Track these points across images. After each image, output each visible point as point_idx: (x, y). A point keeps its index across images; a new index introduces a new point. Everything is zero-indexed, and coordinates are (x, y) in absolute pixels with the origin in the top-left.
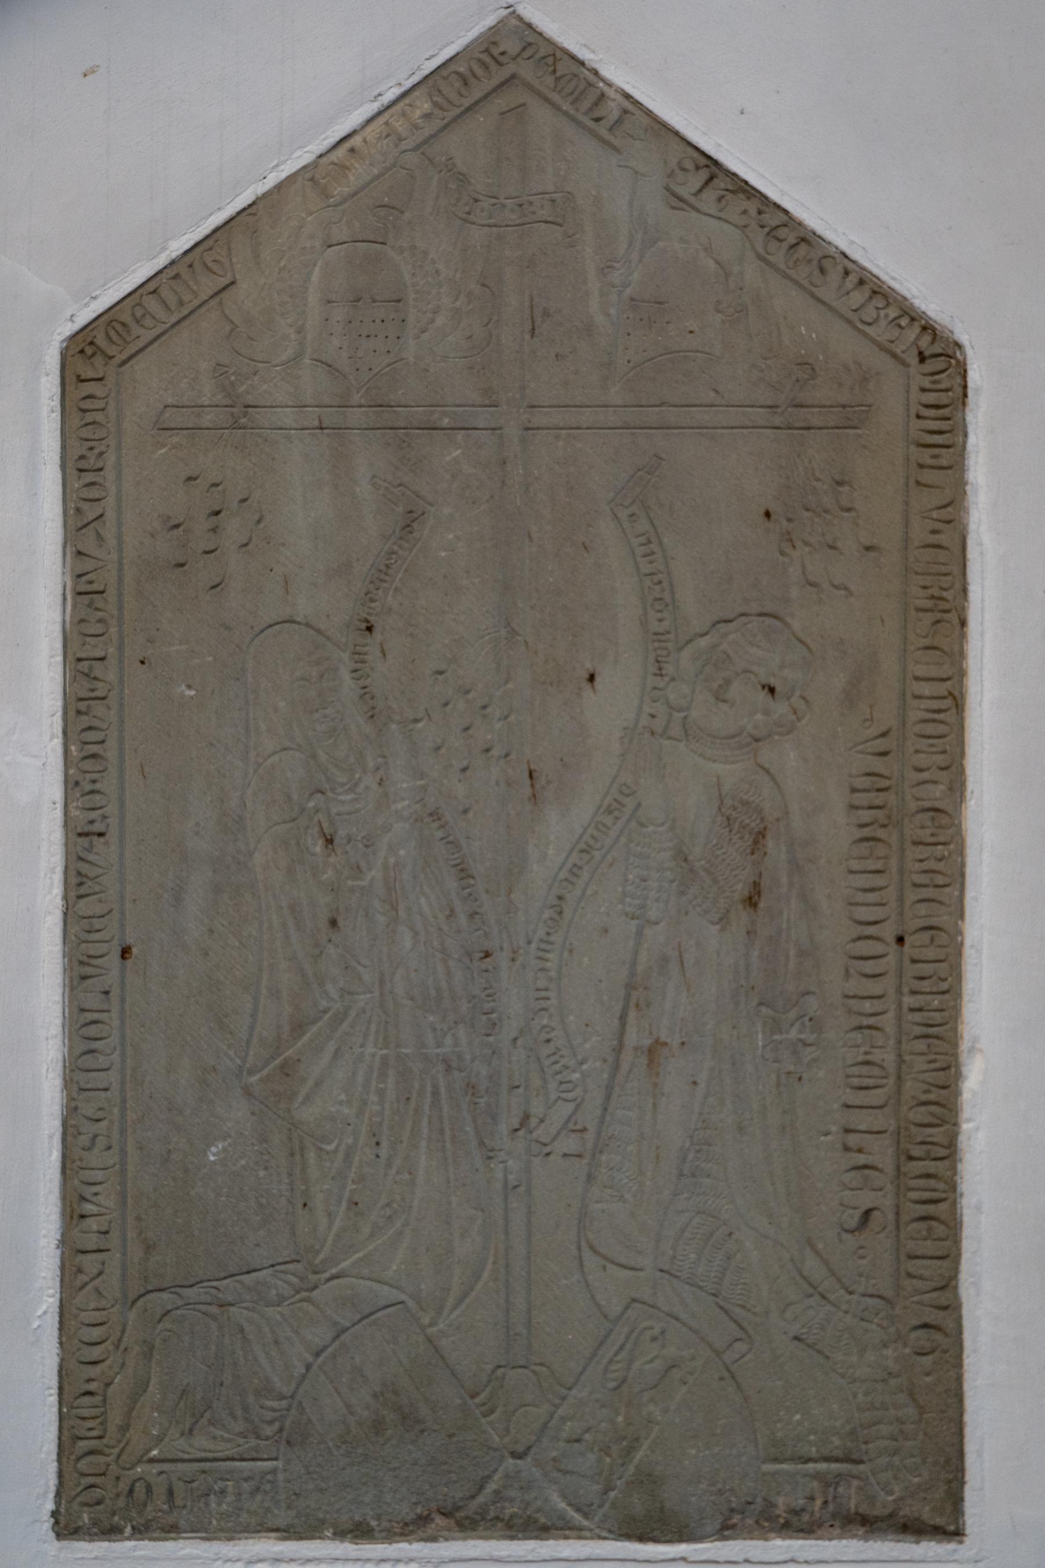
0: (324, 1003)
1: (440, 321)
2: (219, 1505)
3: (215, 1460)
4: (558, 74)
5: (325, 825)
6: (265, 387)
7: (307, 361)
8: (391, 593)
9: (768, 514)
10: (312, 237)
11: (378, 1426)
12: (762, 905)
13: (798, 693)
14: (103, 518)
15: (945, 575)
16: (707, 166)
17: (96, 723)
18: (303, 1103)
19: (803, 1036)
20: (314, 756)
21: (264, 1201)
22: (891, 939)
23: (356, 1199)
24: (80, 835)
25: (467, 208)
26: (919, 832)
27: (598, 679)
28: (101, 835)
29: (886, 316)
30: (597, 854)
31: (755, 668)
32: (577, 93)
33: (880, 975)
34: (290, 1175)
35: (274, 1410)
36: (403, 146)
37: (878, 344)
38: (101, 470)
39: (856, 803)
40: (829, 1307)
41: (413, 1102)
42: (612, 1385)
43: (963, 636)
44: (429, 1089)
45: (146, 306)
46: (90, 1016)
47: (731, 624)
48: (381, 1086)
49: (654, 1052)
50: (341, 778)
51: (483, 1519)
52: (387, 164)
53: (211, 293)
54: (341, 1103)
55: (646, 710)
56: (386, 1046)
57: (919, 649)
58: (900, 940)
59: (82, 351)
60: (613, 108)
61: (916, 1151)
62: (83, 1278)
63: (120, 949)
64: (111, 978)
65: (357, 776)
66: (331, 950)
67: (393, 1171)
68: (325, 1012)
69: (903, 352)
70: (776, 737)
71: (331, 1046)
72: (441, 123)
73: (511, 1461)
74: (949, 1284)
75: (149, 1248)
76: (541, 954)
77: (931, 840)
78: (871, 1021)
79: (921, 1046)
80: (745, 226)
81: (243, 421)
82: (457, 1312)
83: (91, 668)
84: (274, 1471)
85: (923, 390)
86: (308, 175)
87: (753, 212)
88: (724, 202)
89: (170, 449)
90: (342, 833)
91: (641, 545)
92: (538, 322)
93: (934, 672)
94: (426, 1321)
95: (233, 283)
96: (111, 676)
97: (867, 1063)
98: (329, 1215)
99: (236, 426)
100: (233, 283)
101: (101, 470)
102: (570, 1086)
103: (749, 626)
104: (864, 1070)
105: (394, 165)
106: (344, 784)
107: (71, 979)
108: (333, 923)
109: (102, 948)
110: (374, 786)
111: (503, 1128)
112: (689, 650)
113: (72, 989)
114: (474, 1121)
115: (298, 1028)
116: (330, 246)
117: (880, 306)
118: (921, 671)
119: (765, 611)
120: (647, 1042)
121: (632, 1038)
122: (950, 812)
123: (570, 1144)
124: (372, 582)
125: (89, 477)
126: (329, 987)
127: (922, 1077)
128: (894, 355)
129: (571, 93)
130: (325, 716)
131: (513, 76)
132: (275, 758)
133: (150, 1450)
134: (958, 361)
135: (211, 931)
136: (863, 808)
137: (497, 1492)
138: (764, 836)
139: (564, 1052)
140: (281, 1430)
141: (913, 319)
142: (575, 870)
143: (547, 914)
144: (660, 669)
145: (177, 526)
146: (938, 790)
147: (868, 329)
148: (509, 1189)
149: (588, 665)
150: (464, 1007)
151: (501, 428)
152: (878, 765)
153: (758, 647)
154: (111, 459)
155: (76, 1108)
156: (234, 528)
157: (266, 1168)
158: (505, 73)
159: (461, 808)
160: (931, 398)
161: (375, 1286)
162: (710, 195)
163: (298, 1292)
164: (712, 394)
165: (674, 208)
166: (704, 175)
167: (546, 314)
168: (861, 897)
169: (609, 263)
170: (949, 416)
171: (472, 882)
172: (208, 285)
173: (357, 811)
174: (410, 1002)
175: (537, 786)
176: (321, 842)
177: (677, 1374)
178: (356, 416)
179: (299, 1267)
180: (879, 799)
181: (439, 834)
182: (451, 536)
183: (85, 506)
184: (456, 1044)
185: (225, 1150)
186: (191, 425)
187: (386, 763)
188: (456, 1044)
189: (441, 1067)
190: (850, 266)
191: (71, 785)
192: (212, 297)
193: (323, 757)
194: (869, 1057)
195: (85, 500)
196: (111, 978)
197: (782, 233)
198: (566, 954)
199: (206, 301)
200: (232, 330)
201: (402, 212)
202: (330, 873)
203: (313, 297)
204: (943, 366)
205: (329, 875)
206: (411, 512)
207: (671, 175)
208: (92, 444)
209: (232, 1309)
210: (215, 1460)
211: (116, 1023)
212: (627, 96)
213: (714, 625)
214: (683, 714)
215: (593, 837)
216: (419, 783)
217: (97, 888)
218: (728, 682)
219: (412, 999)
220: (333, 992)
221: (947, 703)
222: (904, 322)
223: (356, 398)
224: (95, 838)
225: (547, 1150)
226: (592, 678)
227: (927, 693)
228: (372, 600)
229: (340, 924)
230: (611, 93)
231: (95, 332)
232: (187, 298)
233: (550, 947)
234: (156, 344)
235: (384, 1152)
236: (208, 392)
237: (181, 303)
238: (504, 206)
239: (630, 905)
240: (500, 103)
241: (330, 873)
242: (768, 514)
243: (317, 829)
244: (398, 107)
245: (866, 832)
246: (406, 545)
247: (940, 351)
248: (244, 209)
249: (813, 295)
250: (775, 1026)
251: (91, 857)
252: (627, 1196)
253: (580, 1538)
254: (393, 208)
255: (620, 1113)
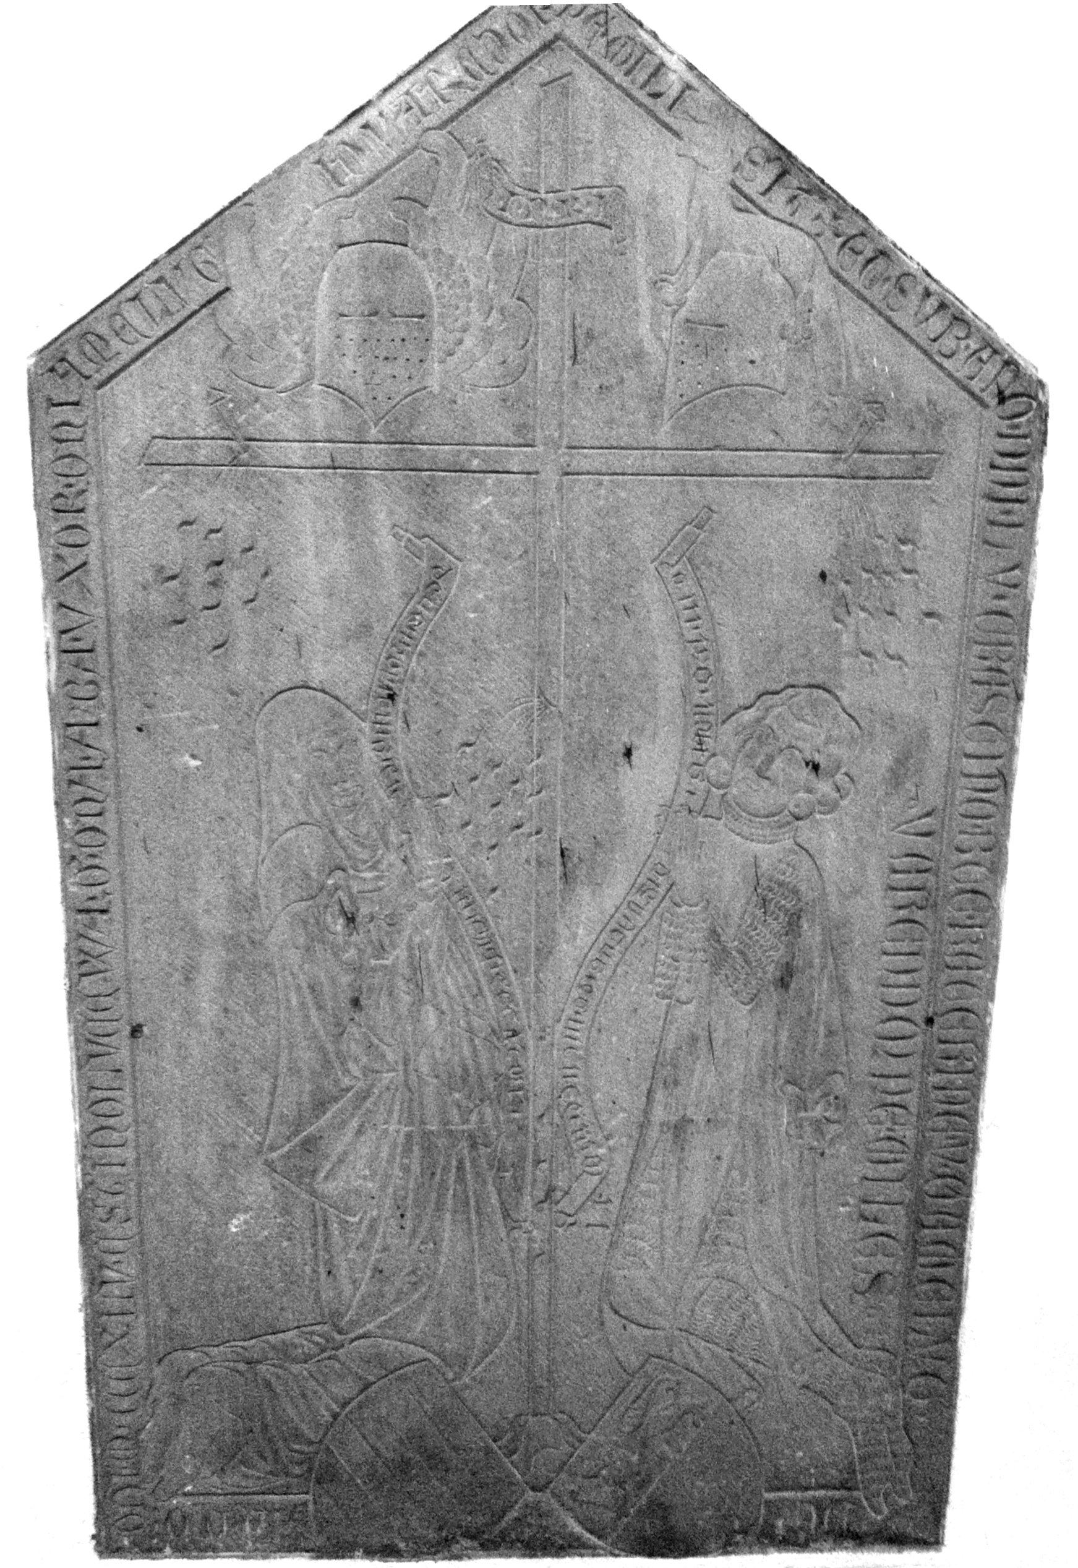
0: (346, 1082)
1: (469, 342)
2: (253, 1529)
3: (248, 1494)
4: (612, 35)
5: (347, 904)
6: (268, 417)
7: (316, 387)
8: (414, 659)
9: (823, 576)
10: (319, 235)
11: (404, 1466)
12: (793, 986)
13: (843, 770)
14: (87, 567)
15: (1004, 645)
16: (779, 159)
17: (91, 793)
18: (326, 1178)
19: (827, 1114)
20: (333, 832)
21: (287, 1269)
22: (920, 1020)
23: (381, 1266)
24: (80, 911)
25: (501, 203)
26: (956, 914)
27: (635, 754)
28: (103, 911)
29: (967, 347)
30: (629, 935)
31: (800, 744)
32: (632, 61)
33: (906, 1055)
34: (313, 1245)
35: (302, 1453)
36: (427, 122)
37: (957, 382)
38: (82, 510)
39: (894, 884)
40: (835, 1359)
41: (438, 1177)
42: (627, 1429)
43: (1017, 711)
44: (454, 1163)
45: (126, 315)
46: (100, 1094)
47: (777, 697)
48: (406, 1161)
49: (679, 1129)
50: (364, 855)
51: (504, 1540)
52: (408, 146)
53: (202, 302)
54: (365, 1178)
55: (684, 786)
56: (412, 1124)
57: (972, 725)
58: (930, 1021)
59: (52, 370)
60: (672, 82)
61: (931, 1220)
62: (107, 1338)
63: (128, 1028)
64: (123, 1056)
65: (380, 852)
66: (354, 1029)
67: (418, 1242)
68: (348, 1090)
69: (983, 390)
70: (818, 816)
71: (354, 1123)
72: (471, 95)
73: (531, 1493)
74: (950, 1337)
75: (173, 1311)
76: (568, 1032)
77: (969, 922)
78: (896, 1099)
79: (941, 1122)
80: (818, 235)
81: (245, 456)
82: (479, 1368)
83: (82, 734)
84: (305, 1504)
85: (1001, 435)
86: (313, 157)
87: (827, 216)
88: (796, 203)
89: (160, 489)
90: (364, 910)
91: (686, 608)
92: (580, 346)
93: (982, 750)
94: (450, 1375)
95: (227, 289)
96: (107, 744)
97: (889, 1138)
98: (354, 1282)
99: (235, 462)
100: (227, 289)
101: (82, 510)
102: (596, 1160)
103: (795, 699)
104: (886, 1145)
105: (416, 147)
106: (366, 862)
107: (78, 1058)
108: (356, 1003)
109: (110, 1027)
110: (399, 863)
111: (527, 1201)
112: (729, 727)
113: (80, 1067)
114: (499, 1194)
115: (320, 1105)
116: (341, 247)
117: (962, 335)
118: (970, 747)
119: (813, 682)
120: (673, 1119)
121: (659, 1114)
122: (988, 892)
123: (594, 1215)
124: (393, 645)
125: (69, 519)
126: (351, 1065)
127: (940, 1151)
128: (972, 394)
129: (625, 62)
130: (344, 790)
131: (557, 37)
132: (290, 835)
133: (185, 1485)
134: (1040, 404)
135: (226, 1010)
136: (902, 889)
137: (517, 1519)
138: (799, 918)
139: (591, 1128)
140: (310, 1470)
141: (995, 352)
142: (606, 950)
143: (575, 993)
144: (701, 744)
145: (173, 577)
146: (978, 872)
147: (946, 363)
148: (532, 1258)
149: (625, 739)
150: (491, 1085)
151: (537, 473)
152: (921, 844)
153: (806, 721)
154: (92, 498)
155: (92, 1183)
156: (237, 584)
157: (289, 1239)
158: (547, 34)
159: (489, 886)
160: (1008, 445)
161: (403, 1346)
162: (780, 196)
163: (323, 1351)
164: (772, 437)
165: (740, 210)
166: (774, 170)
167: (590, 335)
168: (893, 979)
169: (664, 276)
170: (1023, 465)
171: (500, 961)
172: (197, 291)
173: (380, 889)
174: (435, 1081)
175: (570, 865)
176: (341, 921)
177: (689, 1418)
178: (373, 454)
179: (326, 1328)
180: (917, 880)
181: (466, 913)
182: (481, 596)
183: (65, 551)
184: (481, 1121)
185: (246, 1222)
186: (183, 460)
187: (411, 840)
188: (481, 1121)
189: (464, 1144)
190: (933, 287)
191: (68, 859)
192: (203, 306)
193: (341, 833)
194: (891, 1134)
195: (64, 545)
196: (123, 1056)
197: (859, 244)
198: (594, 1033)
199: (194, 313)
200: (228, 347)
201: (426, 207)
202: (352, 951)
203: (322, 308)
204: (1022, 408)
205: (351, 954)
206: (436, 567)
207: (737, 168)
208: (72, 480)
209: (259, 1367)
210: (248, 1494)
211: (129, 1101)
212: (691, 67)
213: (759, 697)
214: (722, 792)
215: (625, 916)
216: (446, 860)
217: (101, 967)
218: (770, 759)
219: (437, 1077)
220: (355, 1070)
221: (997, 781)
222: (985, 355)
223: (373, 432)
224: (97, 915)
225: (571, 1220)
226: (628, 753)
227: (976, 771)
228: (395, 666)
229: (363, 1002)
230: (671, 61)
231: (67, 346)
232: (174, 306)
233: (578, 1026)
234: (139, 363)
235: (408, 1224)
236: (202, 421)
237: (167, 312)
238: (544, 201)
239: (660, 985)
240: (542, 71)
241: (352, 951)
242: (823, 576)
243: (337, 907)
244: (420, 74)
245: (902, 913)
246: (431, 604)
247: (1021, 390)
248: (239, 199)
249: (889, 320)
250: (801, 1104)
251: (93, 934)
252: (649, 1263)
253: (593, 1556)
254: (415, 201)
255: (643, 1186)
